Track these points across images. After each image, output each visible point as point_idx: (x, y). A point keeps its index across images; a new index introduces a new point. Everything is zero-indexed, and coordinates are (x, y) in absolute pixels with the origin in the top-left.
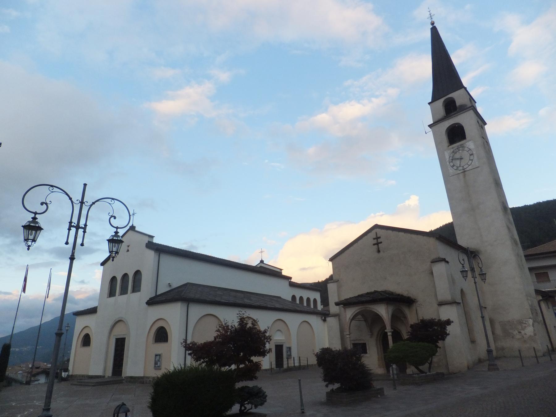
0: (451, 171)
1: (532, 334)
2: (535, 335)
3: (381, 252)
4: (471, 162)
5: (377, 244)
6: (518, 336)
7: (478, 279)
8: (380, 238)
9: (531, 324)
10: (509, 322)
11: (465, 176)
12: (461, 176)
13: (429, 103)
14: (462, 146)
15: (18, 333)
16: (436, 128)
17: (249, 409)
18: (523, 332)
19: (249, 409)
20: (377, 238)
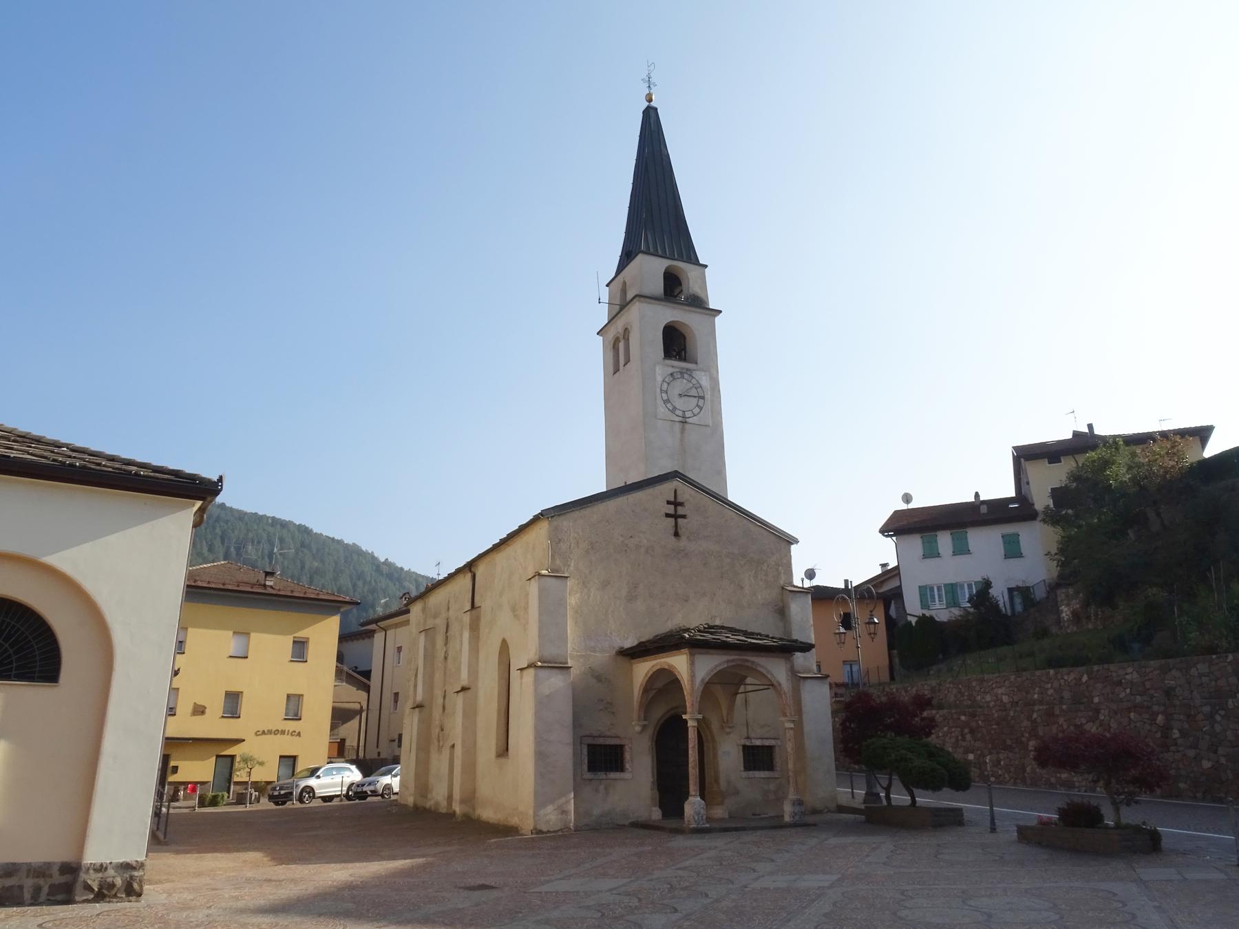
0: (662, 410)
3: (683, 538)
8: (681, 504)
11: (683, 430)
12: (678, 427)
15: (241, 516)
20: (676, 504)
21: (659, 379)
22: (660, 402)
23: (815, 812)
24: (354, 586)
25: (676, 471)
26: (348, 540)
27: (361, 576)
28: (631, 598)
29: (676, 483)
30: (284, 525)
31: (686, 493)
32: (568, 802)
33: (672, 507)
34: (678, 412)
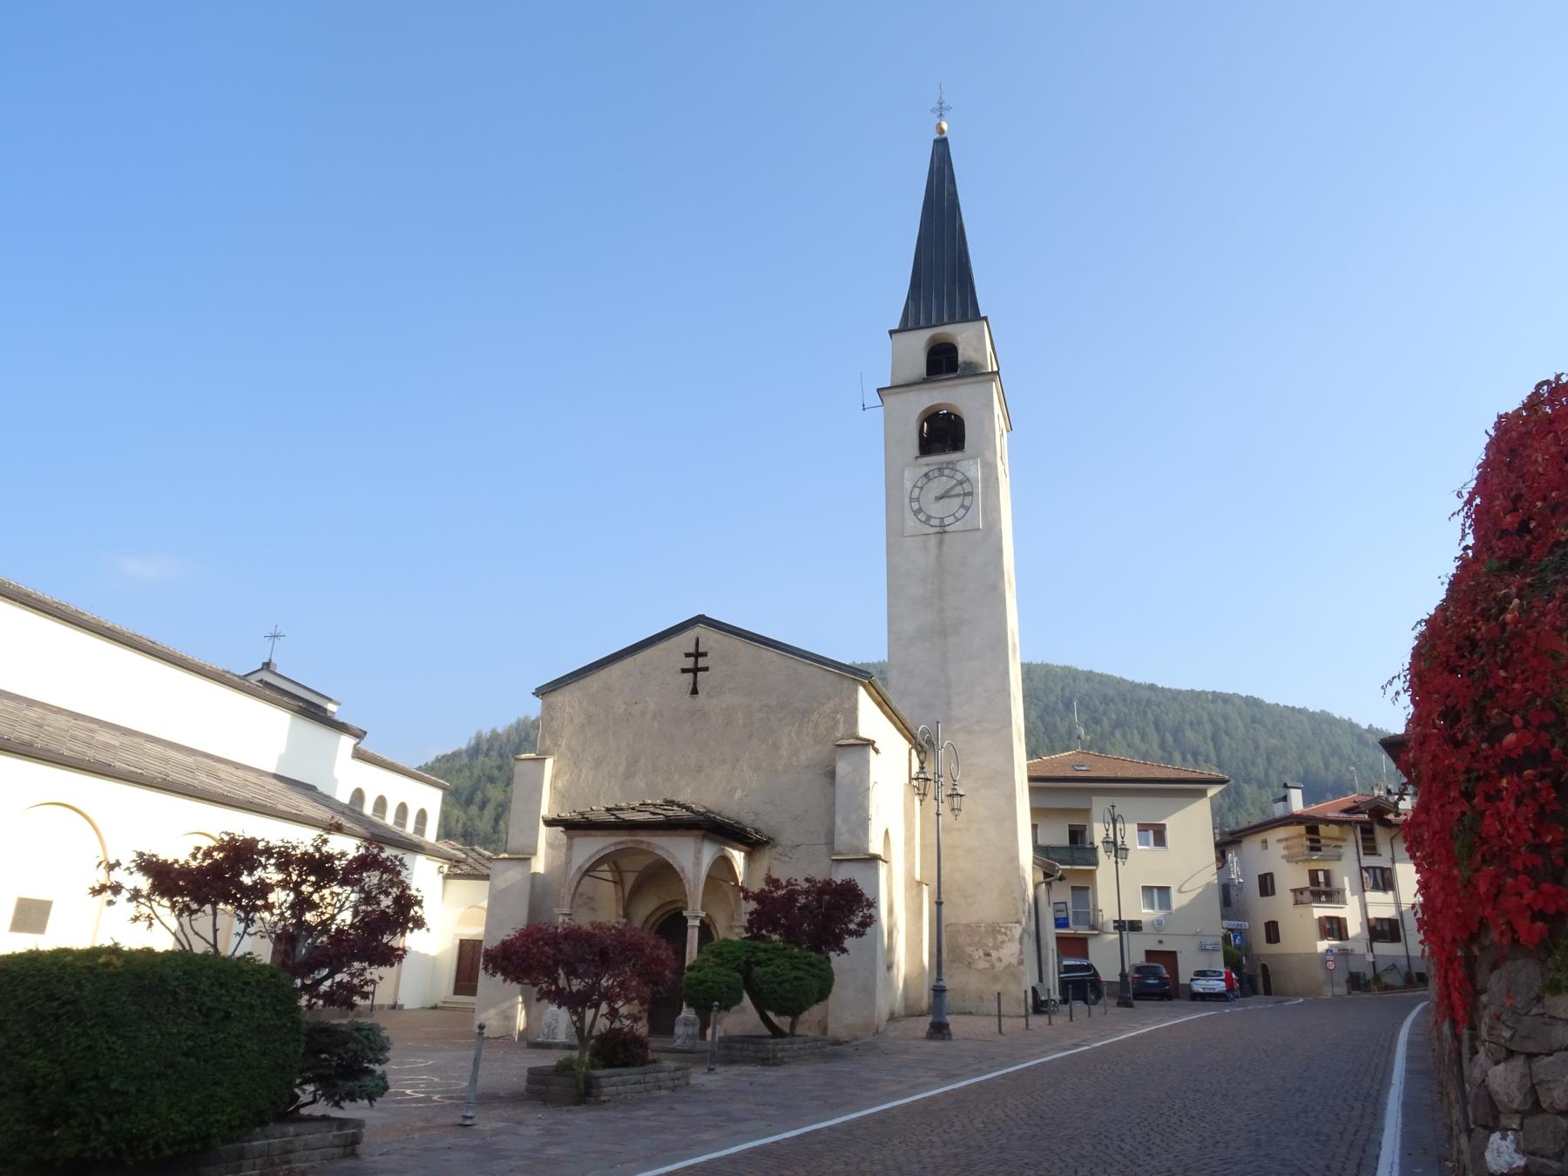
0: (911, 523)
1: (1014, 961)
2: (1021, 963)
3: (701, 695)
4: (962, 511)
5: (695, 670)
6: (982, 964)
7: (945, 808)
8: (705, 654)
9: (1017, 936)
10: (968, 926)
11: (940, 544)
12: (933, 541)
13: (892, 332)
14: (951, 466)
16: (894, 400)
17: (305, 1105)
18: (994, 954)
19: (305, 1105)
20: (697, 655)
21: (908, 485)
22: (909, 515)
23: (837, 1042)
24: (1327, 765)
25: (702, 617)
26: (1314, 707)
27: (1336, 750)
28: (629, 775)
29: (699, 630)
30: (1226, 699)
31: (709, 639)
32: (514, 1007)
33: (700, 665)
34: (933, 522)
